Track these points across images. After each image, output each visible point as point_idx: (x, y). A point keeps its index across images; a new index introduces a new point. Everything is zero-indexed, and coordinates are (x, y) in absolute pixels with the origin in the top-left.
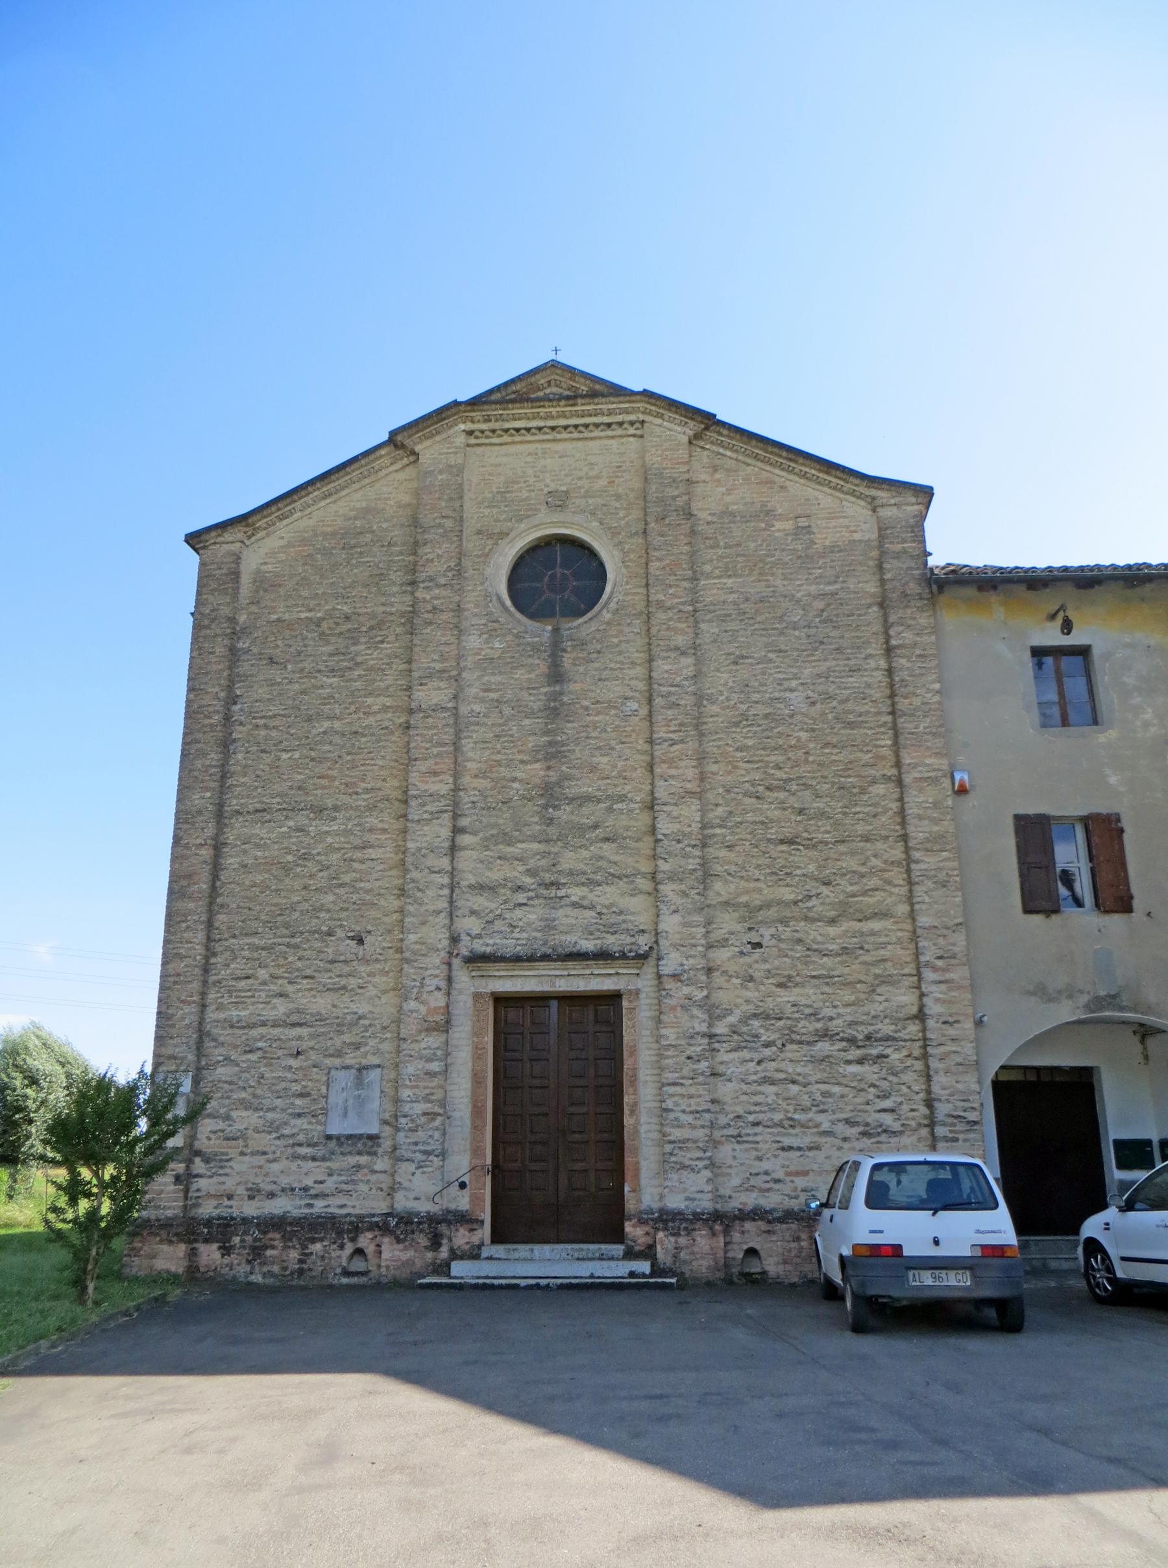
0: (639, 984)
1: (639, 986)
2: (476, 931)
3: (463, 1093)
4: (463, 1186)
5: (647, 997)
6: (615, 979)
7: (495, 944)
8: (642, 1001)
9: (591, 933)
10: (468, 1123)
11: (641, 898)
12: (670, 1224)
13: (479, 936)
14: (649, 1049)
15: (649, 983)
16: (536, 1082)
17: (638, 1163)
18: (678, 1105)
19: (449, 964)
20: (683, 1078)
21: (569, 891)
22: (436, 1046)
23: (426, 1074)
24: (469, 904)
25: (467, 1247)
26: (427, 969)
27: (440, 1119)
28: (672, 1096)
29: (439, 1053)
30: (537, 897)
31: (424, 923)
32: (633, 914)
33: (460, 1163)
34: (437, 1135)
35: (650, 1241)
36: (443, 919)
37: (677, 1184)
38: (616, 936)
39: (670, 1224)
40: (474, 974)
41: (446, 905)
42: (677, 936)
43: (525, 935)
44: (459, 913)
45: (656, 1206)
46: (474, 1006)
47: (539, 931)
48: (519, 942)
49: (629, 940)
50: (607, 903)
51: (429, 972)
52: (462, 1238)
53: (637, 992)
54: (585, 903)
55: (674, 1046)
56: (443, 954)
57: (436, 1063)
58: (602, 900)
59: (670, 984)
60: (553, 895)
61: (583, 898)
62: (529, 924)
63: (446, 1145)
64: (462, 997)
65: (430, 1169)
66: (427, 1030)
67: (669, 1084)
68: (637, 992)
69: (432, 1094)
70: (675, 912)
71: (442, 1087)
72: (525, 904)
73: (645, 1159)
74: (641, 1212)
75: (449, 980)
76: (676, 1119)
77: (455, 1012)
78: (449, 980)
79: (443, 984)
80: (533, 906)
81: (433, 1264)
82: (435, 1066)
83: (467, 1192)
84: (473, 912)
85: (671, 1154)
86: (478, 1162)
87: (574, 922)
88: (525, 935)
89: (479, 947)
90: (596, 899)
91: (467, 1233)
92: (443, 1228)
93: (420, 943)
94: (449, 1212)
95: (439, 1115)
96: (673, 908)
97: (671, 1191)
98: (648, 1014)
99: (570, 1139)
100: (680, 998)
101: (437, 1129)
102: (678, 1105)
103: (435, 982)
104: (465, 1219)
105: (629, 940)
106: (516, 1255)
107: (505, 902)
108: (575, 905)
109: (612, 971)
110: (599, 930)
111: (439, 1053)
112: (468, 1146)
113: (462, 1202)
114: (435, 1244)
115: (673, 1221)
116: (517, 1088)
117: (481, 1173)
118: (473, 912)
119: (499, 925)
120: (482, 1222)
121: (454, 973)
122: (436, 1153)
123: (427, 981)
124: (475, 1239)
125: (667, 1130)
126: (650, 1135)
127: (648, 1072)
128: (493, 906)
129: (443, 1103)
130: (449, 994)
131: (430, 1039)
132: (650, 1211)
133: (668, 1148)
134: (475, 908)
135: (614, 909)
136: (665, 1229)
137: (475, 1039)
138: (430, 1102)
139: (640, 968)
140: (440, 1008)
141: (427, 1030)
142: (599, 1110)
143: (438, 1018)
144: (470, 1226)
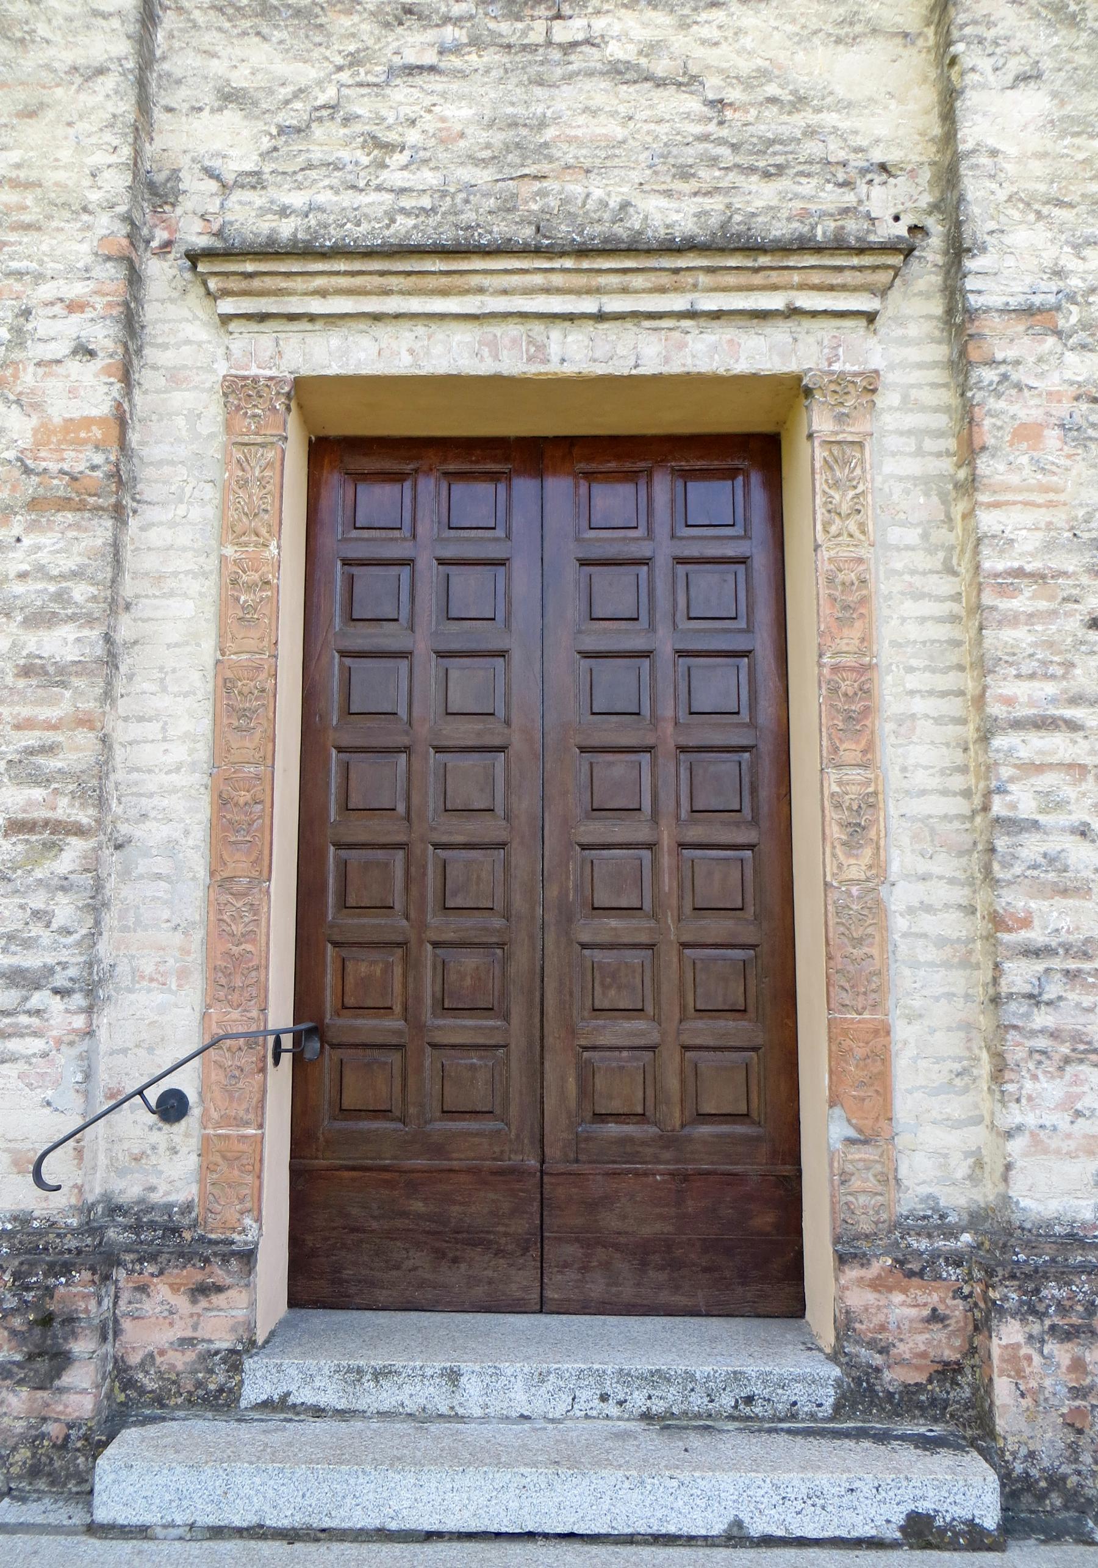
0: (865, 351)
1: (876, 361)
2: (241, 160)
3: (179, 753)
4: (172, 1107)
5: (907, 405)
6: (779, 333)
7: (312, 208)
8: (889, 421)
9: (684, 173)
10: (198, 864)
11: (878, 50)
12: (1052, 1290)
13: (254, 180)
14: (918, 596)
15: (913, 354)
16: (463, 732)
17: (884, 1030)
18: (1060, 805)
19: (135, 278)
20: (1075, 700)
21: (599, 24)
22: (68, 564)
23: (26, 671)
24: (217, 67)
25: (181, 1360)
26: (39, 278)
27: (76, 846)
28: (1038, 768)
29: (80, 592)
30: (476, 42)
31: (30, 113)
32: (846, 106)
33: (162, 1019)
34: (65, 909)
35: (947, 1346)
36: (111, 98)
37: (1061, 1120)
38: (783, 183)
39: (1052, 1290)
40: (227, 306)
41: (123, 47)
42: (1038, 167)
43: (429, 178)
44: (178, 97)
45: (957, 1199)
46: (228, 427)
47: (484, 163)
48: (407, 202)
49: (832, 198)
50: (745, 66)
51: (47, 291)
52: (161, 1322)
53: (870, 385)
54: (661, 67)
55: (1039, 577)
56: (106, 224)
57: (68, 632)
58: (724, 56)
59: (1007, 343)
60: (536, 36)
61: (651, 48)
62: (445, 139)
63: (103, 948)
64: (180, 399)
65: (36, 1045)
66: (34, 504)
67: (1017, 725)
68: (870, 385)
69: (49, 750)
70: (1023, 78)
71: (85, 722)
72: (432, 69)
73: (910, 1019)
74: (900, 1226)
75: (131, 323)
76: (1051, 860)
77: (153, 452)
78: (131, 323)
79: (104, 336)
80: (461, 74)
81: (35, 1440)
82: (62, 643)
83: (186, 1133)
84: (231, 97)
85: (1034, 999)
86: (236, 1020)
87: (620, 133)
88: (429, 178)
89: (249, 217)
90: (699, 52)
91: (181, 1302)
92: (77, 1292)
93: (16, 184)
94: (115, 1209)
95: (79, 831)
96: (1016, 65)
97: (1037, 1145)
98: (913, 467)
99: (585, 938)
100: (1052, 396)
101: (65, 885)
102: (1060, 805)
103: (74, 326)
104: (169, 1242)
105: (832, 198)
106: (386, 1397)
107: (355, 61)
108: (619, 72)
109: (775, 301)
110: (713, 161)
111: (80, 592)
112: (196, 957)
113: (168, 1170)
114: (46, 1359)
115: (1064, 1275)
116: (399, 750)
117: (248, 1059)
118: (231, 97)
119: (327, 141)
120: (248, 1257)
121: (151, 312)
122: (60, 980)
123: (41, 325)
124: (219, 1324)
125: (1014, 901)
126: (928, 923)
127: (912, 682)
128: (308, 74)
129: (95, 786)
130: (126, 378)
131: (48, 540)
132: (936, 1223)
133: (1019, 975)
134: (240, 79)
135: (772, 90)
136: (1031, 1310)
137: (230, 551)
138: (38, 779)
139: (883, 292)
140: (88, 422)
141: (34, 504)
142: (695, 833)
143: (78, 460)
144: (193, 1275)
